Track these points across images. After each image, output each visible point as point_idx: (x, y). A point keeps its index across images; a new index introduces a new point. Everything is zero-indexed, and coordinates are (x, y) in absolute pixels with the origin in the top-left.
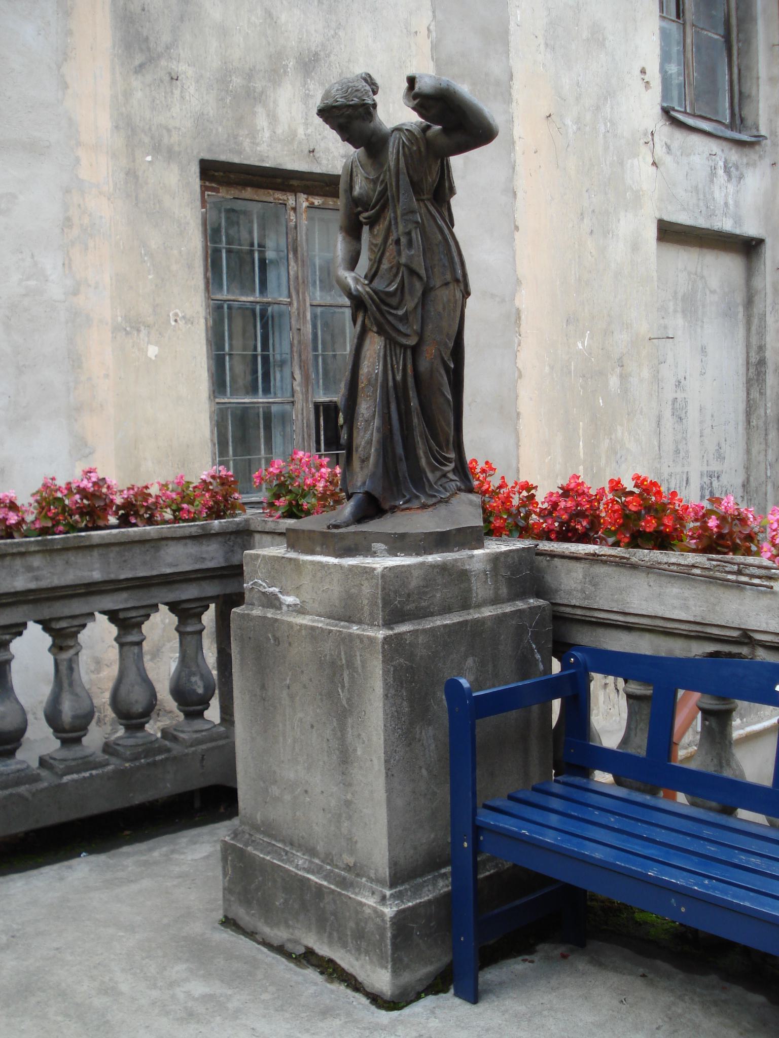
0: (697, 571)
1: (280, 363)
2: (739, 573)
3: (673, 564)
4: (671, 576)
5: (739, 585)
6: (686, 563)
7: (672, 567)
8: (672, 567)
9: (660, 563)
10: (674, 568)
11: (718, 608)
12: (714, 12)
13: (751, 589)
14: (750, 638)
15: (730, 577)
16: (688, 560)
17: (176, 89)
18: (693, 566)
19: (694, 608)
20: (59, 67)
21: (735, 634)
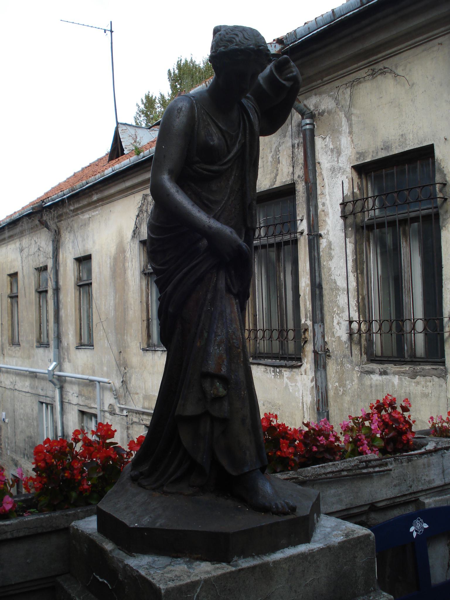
0: (345, 473)
1: (44, 483)
2: (367, 467)
3: (329, 473)
4: (328, 482)
5: (369, 475)
6: (337, 469)
7: (328, 476)
8: (328, 476)
9: (320, 475)
10: (331, 475)
11: (359, 494)
12: (36, 502)
13: (376, 475)
14: (376, 507)
15: (365, 471)
16: (339, 467)
17: (224, 49)
18: (343, 470)
19: (345, 500)
20: (128, 428)
21: (366, 508)
